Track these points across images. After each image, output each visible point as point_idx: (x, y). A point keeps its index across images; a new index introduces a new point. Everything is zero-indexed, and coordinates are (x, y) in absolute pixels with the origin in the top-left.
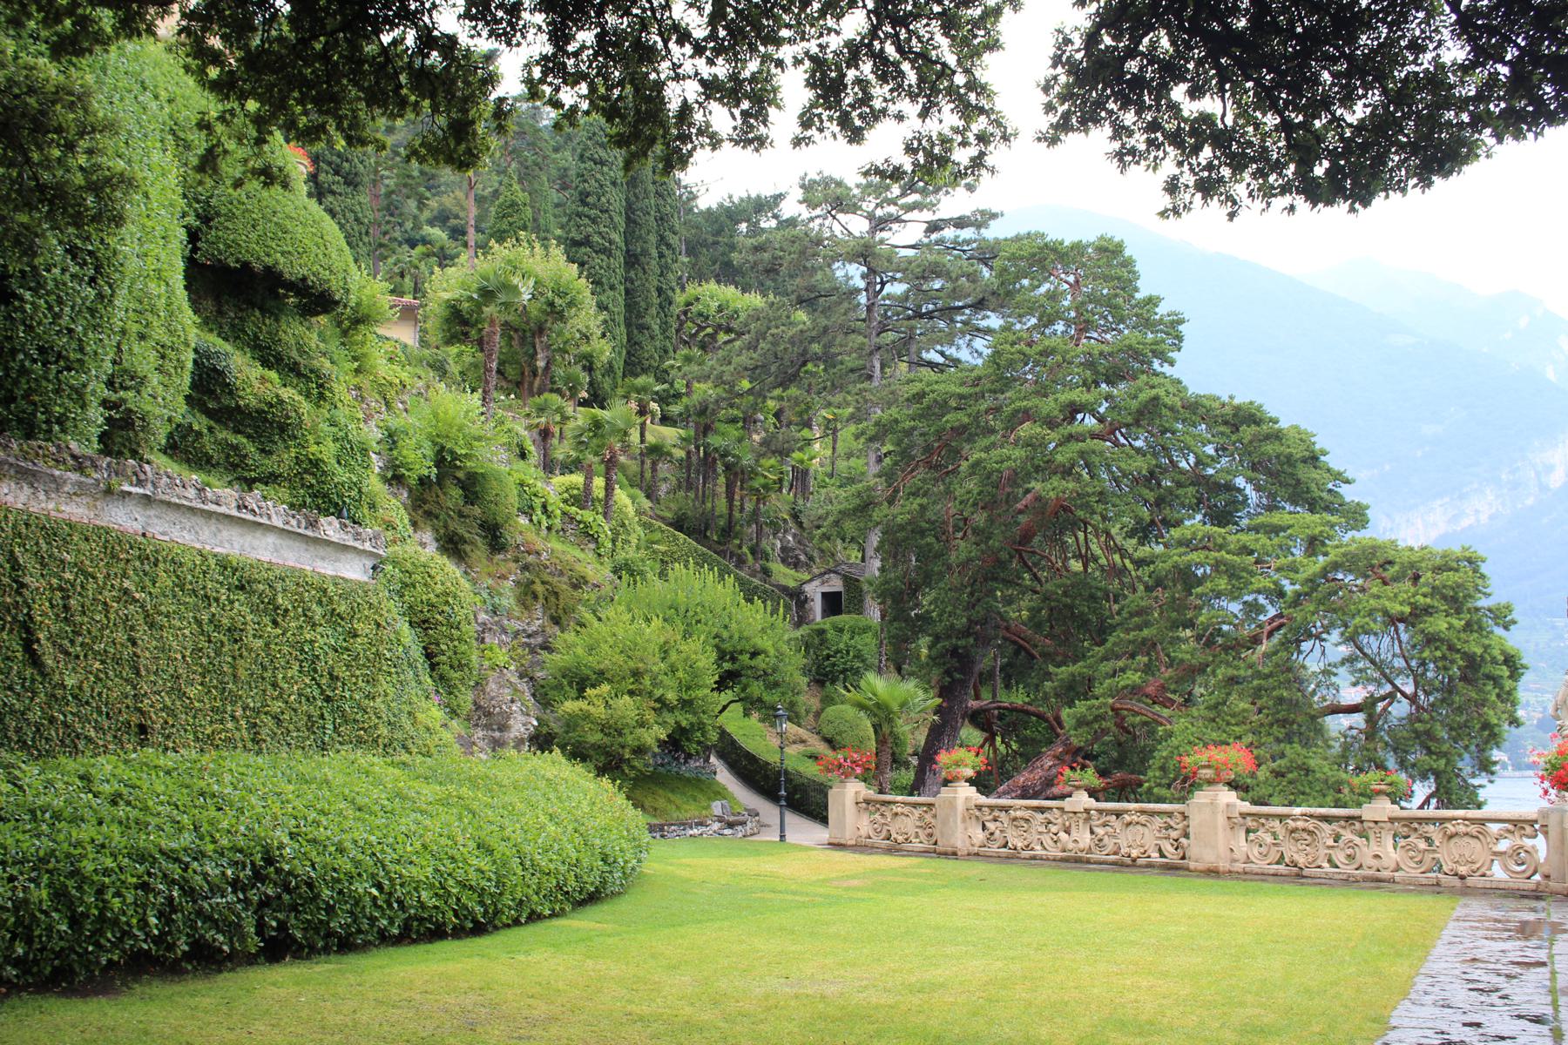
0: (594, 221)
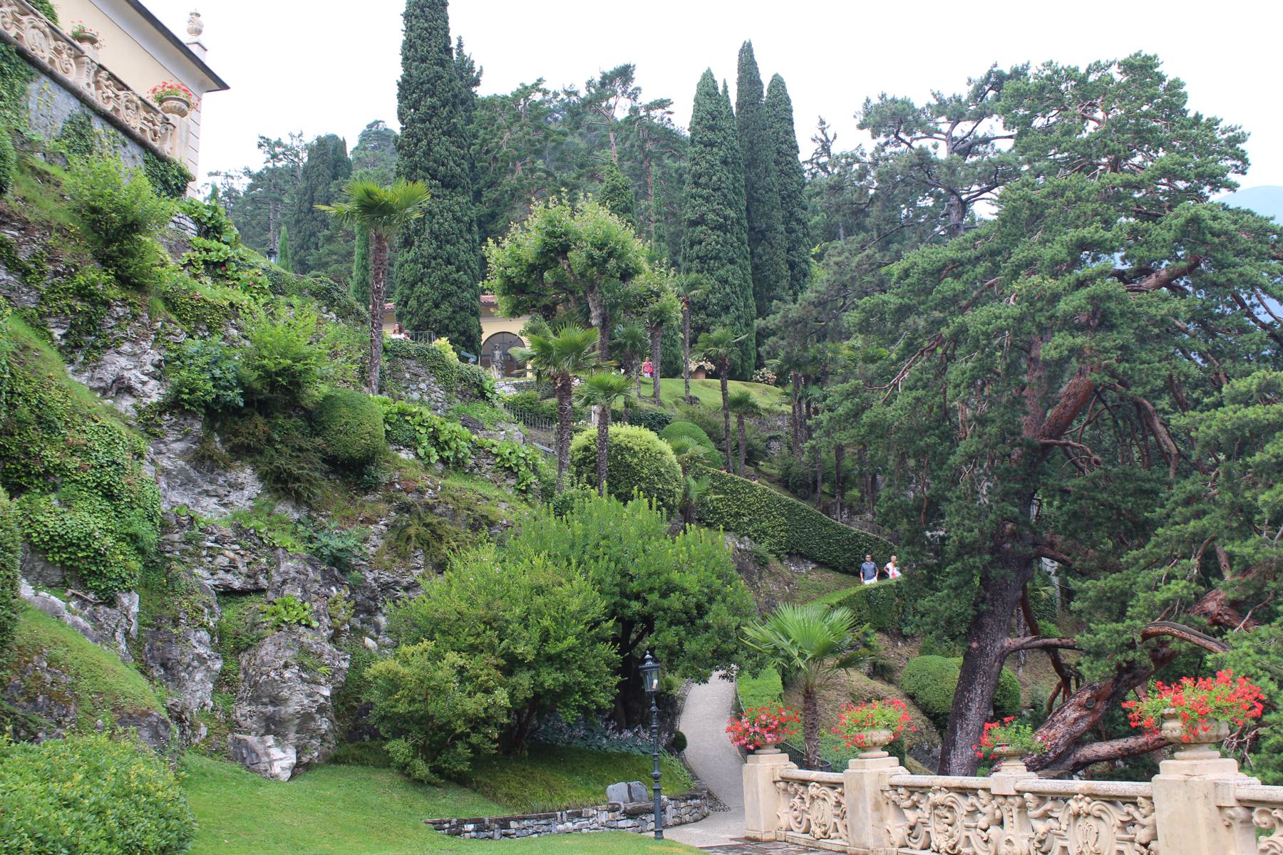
0: (707, 200)
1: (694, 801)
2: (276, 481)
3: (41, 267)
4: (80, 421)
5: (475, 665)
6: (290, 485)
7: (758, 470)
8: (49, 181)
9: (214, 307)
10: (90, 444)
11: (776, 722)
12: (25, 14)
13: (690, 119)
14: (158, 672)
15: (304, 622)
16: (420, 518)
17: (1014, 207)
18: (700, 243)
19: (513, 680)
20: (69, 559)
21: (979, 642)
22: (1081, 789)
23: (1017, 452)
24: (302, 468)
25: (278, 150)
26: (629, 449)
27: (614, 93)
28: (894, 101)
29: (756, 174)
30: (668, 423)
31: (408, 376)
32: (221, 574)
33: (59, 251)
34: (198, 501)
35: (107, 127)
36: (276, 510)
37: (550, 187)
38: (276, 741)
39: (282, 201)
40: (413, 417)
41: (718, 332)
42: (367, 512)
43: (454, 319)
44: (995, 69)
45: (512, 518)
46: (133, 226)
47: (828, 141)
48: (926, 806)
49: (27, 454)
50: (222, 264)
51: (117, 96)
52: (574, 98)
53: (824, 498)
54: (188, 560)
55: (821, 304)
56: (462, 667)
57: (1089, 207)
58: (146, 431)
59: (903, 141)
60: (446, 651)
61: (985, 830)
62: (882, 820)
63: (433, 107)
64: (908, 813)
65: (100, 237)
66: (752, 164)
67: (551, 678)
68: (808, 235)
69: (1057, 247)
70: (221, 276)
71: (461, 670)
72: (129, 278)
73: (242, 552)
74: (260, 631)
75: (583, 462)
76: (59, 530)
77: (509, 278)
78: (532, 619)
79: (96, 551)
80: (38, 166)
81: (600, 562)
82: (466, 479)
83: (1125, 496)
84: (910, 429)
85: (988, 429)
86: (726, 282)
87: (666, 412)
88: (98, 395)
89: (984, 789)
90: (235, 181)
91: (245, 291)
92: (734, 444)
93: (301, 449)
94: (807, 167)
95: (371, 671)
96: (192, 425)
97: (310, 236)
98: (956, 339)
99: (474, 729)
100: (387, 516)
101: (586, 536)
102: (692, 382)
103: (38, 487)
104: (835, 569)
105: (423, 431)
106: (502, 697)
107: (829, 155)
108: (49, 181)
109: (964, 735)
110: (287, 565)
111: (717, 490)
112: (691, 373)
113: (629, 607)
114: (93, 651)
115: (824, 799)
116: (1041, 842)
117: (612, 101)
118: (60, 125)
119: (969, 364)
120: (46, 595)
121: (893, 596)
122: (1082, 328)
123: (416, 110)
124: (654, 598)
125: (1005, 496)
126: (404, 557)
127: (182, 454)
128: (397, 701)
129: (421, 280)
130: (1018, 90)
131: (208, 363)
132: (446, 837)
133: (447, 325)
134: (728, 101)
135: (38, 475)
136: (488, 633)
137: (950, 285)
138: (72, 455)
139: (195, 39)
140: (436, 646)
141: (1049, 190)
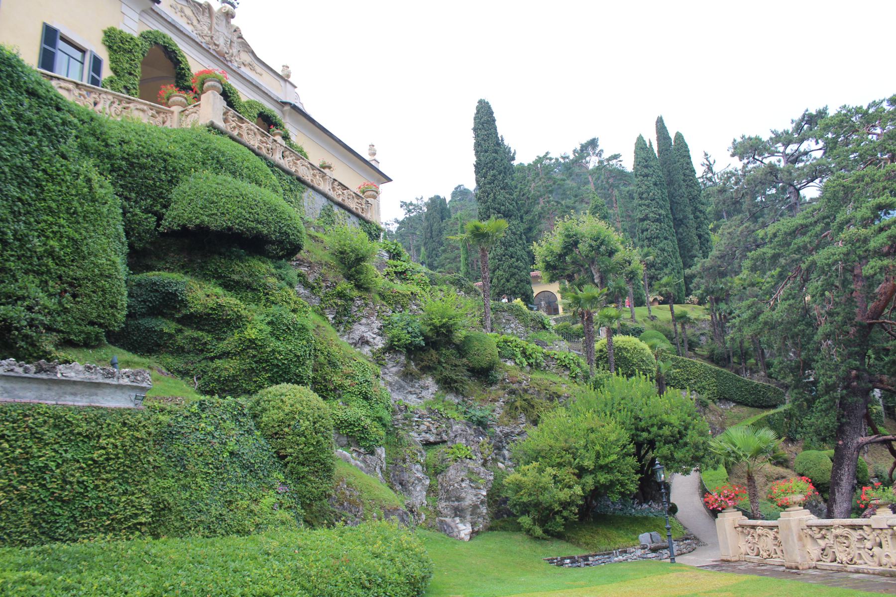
0: (648, 206)
2: (444, 384)
5: (562, 473)
7: (695, 353)
9: (404, 295)
11: (733, 494)
12: (298, 160)
13: (633, 163)
14: (399, 487)
16: (521, 397)
18: (647, 230)
19: (583, 481)
20: (350, 432)
23: (852, 330)
24: (458, 375)
25: (411, 207)
27: (589, 155)
28: (750, 139)
30: (642, 332)
31: (504, 321)
32: (423, 434)
35: (340, 209)
37: (565, 211)
38: (461, 520)
39: (416, 234)
41: (665, 280)
42: (493, 396)
45: (570, 392)
46: (360, 259)
47: (710, 164)
49: (325, 380)
50: (403, 273)
52: (567, 160)
53: (735, 366)
54: (406, 428)
55: (722, 257)
58: (377, 363)
59: (758, 160)
60: (546, 467)
61: (871, 550)
62: (804, 546)
63: (494, 176)
66: (670, 183)
67: (603, 478)
68: (706, 218)
69: (864, 210)
70: (404, 279)
71: (555, 476)
75: (600, 358)
77: (547, 262)
79: (363, 427)
81: (622, 412)
84: (788, 323)
87: (640, 326)
90: (391, 226)
92: (681, 340)
93: (456, 366)
95: (507, 480)
98: (809, 270)
99: (564, 508)
101: (612, 399)
102: (652, 307)
104: (747, 405)
105: (518, 350)
106: (578, 490)
107: (712, 172)
110: (456, 427)
111: (676, 366)
112: (650, 303)
114: (367, 478)
117: (588, 159)
118: (319, 212)
119: (819, 282)
122: (887, 255)
123: (485, 178)
124: (654, 429)
125: (850, 355)
127: (397, 373)
128: (522, 495)
129: (498, 268)
130: (827, 124)
134: (653, 150)
135: (331, 390)
136: (568, 456)
137: (800, 240)
141: (854, 178)
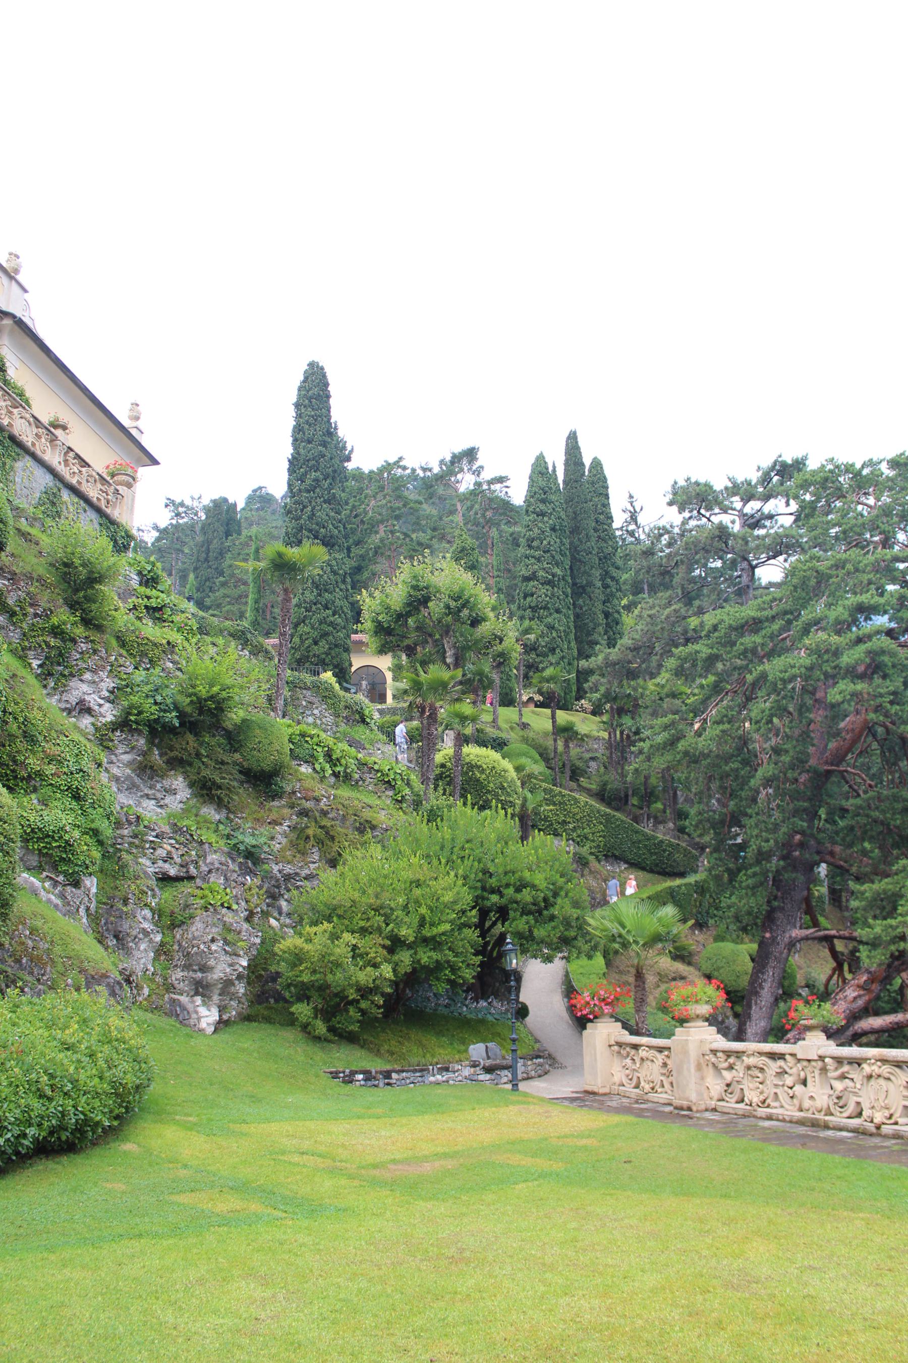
0: (538, 560)
1: (539, 1060)
2: (201, 789)
3: (25, 609)
4: (55, 736)
5: (364, 943)
6: (213, 792)
7: (579, 786)
8: (30, 541)
10: (63, 755)
11: (612, 997)
13: (525, 493)
14: (112, 942)
15: (226, 905)
16: (316, 821)
17: (805, 576)
18: (532, 595)
19: (396, 958)
20: (45, 847)
21: (771, 933)
22: (874, 1056)
23: (803, 778)
24: (224, 778)
25: (181, 510)
26: (478, 767)
27: (462, 470)
28: (697, 484)
29: (579, 539)
30: (505, 745)
31: (304, 703)
32: (160, 863)
33: (38, 597)
34: (140, 803)
36: (202, 812)
37: (416, 550)
38: (203, 1001)
39: (183, 552)
40: (312, 738)
42: (274, 816)
43: (330, 654)
44: (780, 459)
46: (94, 579)
47: (635, 512)
48: (739, 1067)
49: (15, 761)
50: (159, 609)
51: (80, 472)
52: (428, 474)
53: (634, 810)
54: (134, 851)
55: (635, 649)
56: (355, 946)
57: (865, 578)
58: (101, 744)
59: (703, 516)
60: (342, 932)
61: (791, 1088)
63: (316, 480)
64: (725, 1073)
65: (70, 586)
66: (575, 530)
67: (426, 957)
68: (620, 590)
69: (840, 609)
70: (159, 619)
71: (355, 947)
72: (90, 620)
73: (177, 846)
74: (191, 911)
75: (440, 777)
76: (39, 824)
77: (379, 622)
78: (411, 907)
79: (67, 842)
80: (23, 528)
81: (466, 862)
82: (353, 790)
83: (894, 814)
84: (717, 756)
85: (783, 758)
86: (553, 628)
87: (504, 735)
88: (65, 714)
89: (791, 1055)
91: (178, 631)
92: (561, 764)
94: (618, 533)
95: (281, 946)
96: (137, 741)
97: (206, 581)
100: (290, 819)
101: (453, 839)
102: (524, 710)
103: (22, 788)
104: (643, 869)
105: (319, 749)
108: (30, 541)
109: (758, 1009)
110: (213, 857)
112: (523, 703)
113: (488, 899)
114: (64, 923)
115: (653, 1061)
116: (839, 1098)
117: (459, 476)
120: (27, 876)
121: (692, 892)
122: (862, 677)
123: (302, 482)
124: (511, 891)
125: (796, 813)
126: (303, 853)
127: (129, 764)
128: (301, 971)
129: (304, 622)
131: (151, 691)
132: (341, 1084)
133: (324, 659)
134: (556, 479)
135: (23, 779)
137: (749, 640)
138: (49, 763)
139: (135, 424)
140: (334, 928)
141: (833, 562)
